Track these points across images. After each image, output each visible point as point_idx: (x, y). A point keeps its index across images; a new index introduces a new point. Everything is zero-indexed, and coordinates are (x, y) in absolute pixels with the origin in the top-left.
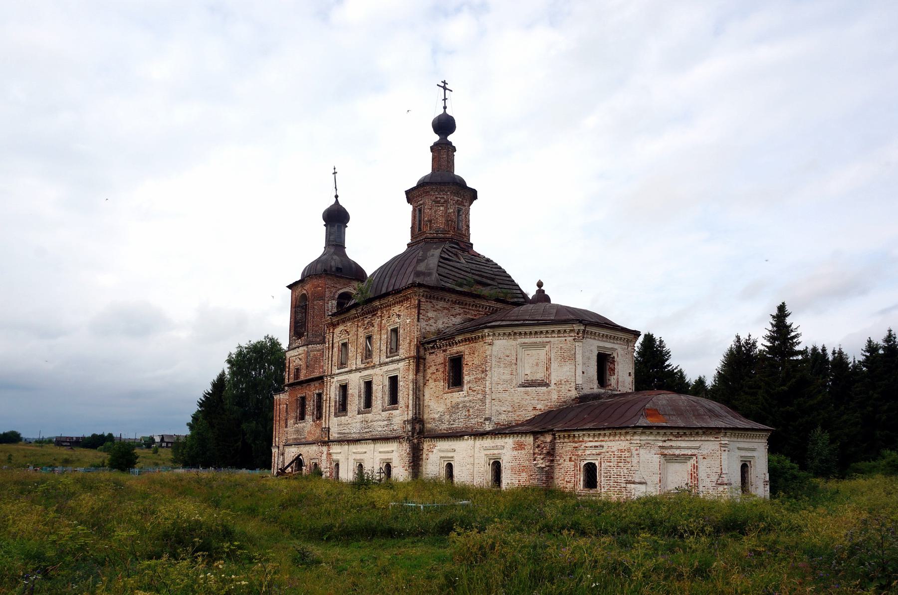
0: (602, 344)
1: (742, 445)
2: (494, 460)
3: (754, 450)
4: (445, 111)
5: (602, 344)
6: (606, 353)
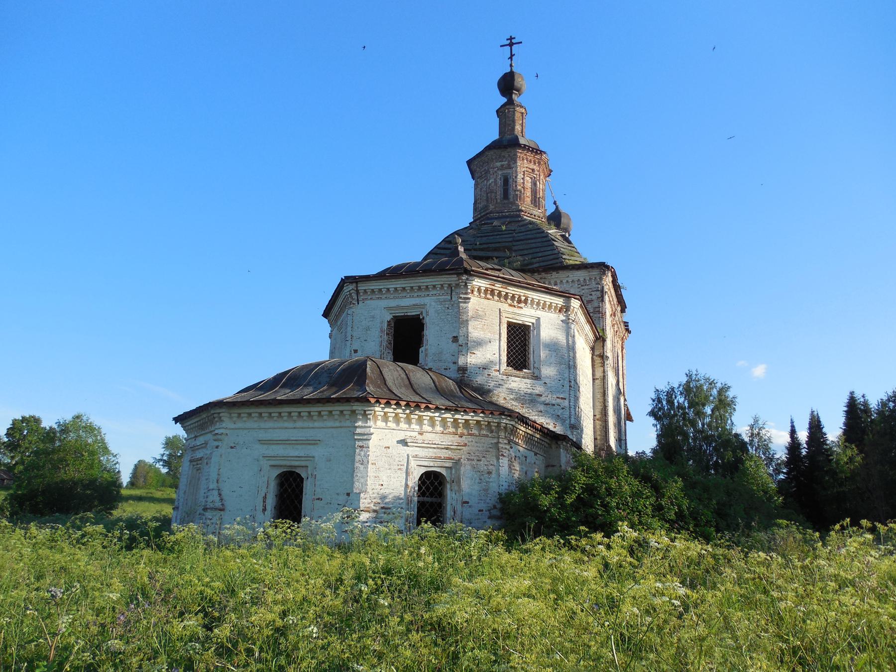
0: (393, 303)
1: (263, 435)
2: (423, 470)
3: (315, 443)
4: (511, 69)
5: (393, 303)
6: (409, 314)
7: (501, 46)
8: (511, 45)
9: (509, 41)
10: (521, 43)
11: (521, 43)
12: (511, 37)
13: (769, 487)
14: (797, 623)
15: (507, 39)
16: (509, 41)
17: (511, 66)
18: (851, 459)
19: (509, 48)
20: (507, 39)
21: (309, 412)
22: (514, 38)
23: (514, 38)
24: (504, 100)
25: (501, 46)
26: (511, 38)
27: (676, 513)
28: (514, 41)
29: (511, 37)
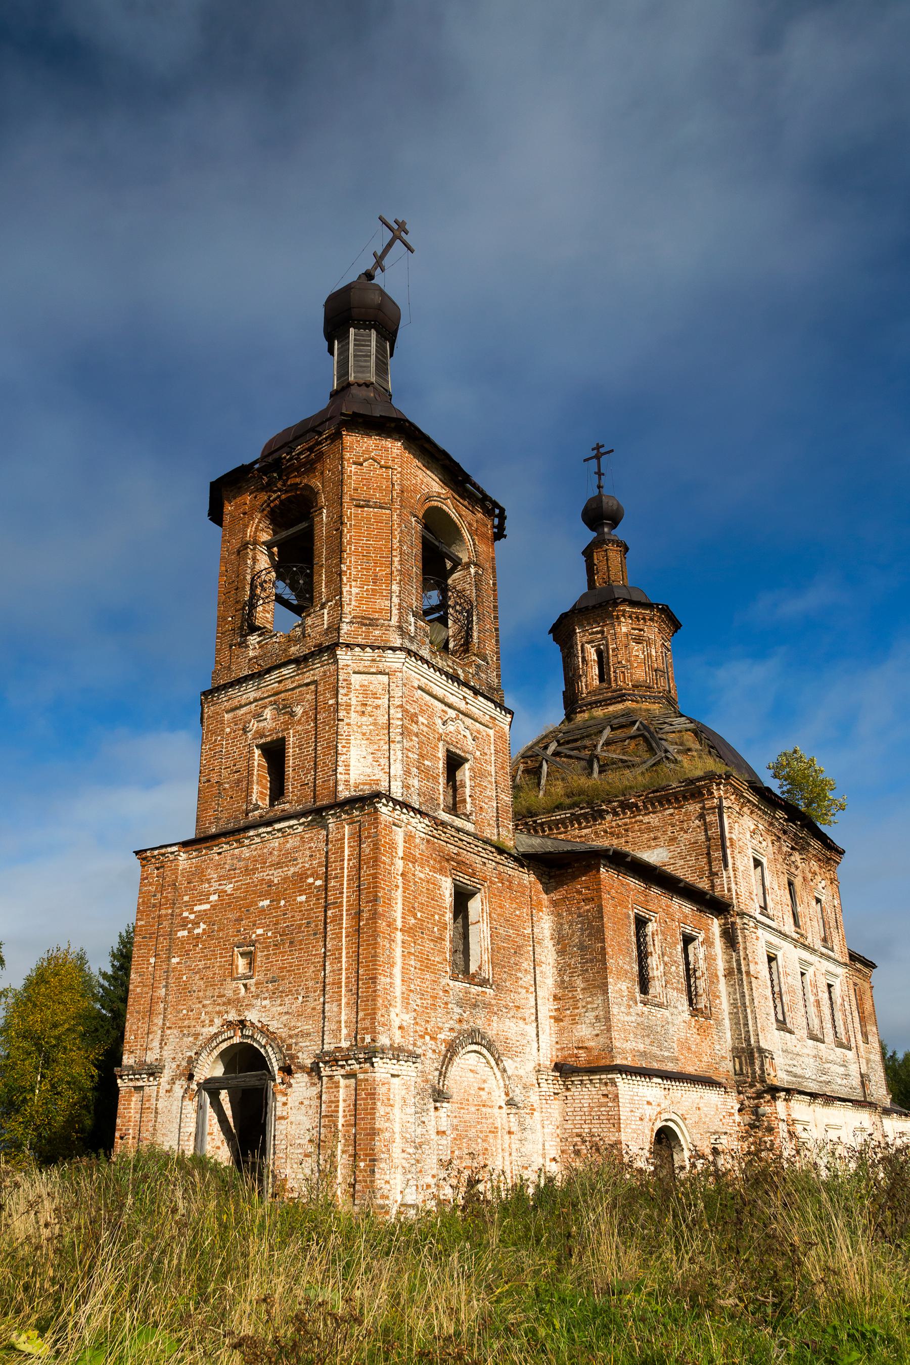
7: (585, 461)
8: (598, 457)
9: (595, 452)
10: (612, 451)
11: (612, 451)
12: (595, 473)
13: (685, 1283)
14: (460, 1185)
15: (593, 449)
16: (595, 452)
17: (600, 474)
18: (33, 1205)
19: (595, 461)
20: (593, 449)
21: (600, 1079)
22: (603, 446)
23: (603, 446)
24: (592, 535)
25: (585, 461)
26: (598, 447)
27: (187, 917)
28: (602, 450)
29: (595, 473)
